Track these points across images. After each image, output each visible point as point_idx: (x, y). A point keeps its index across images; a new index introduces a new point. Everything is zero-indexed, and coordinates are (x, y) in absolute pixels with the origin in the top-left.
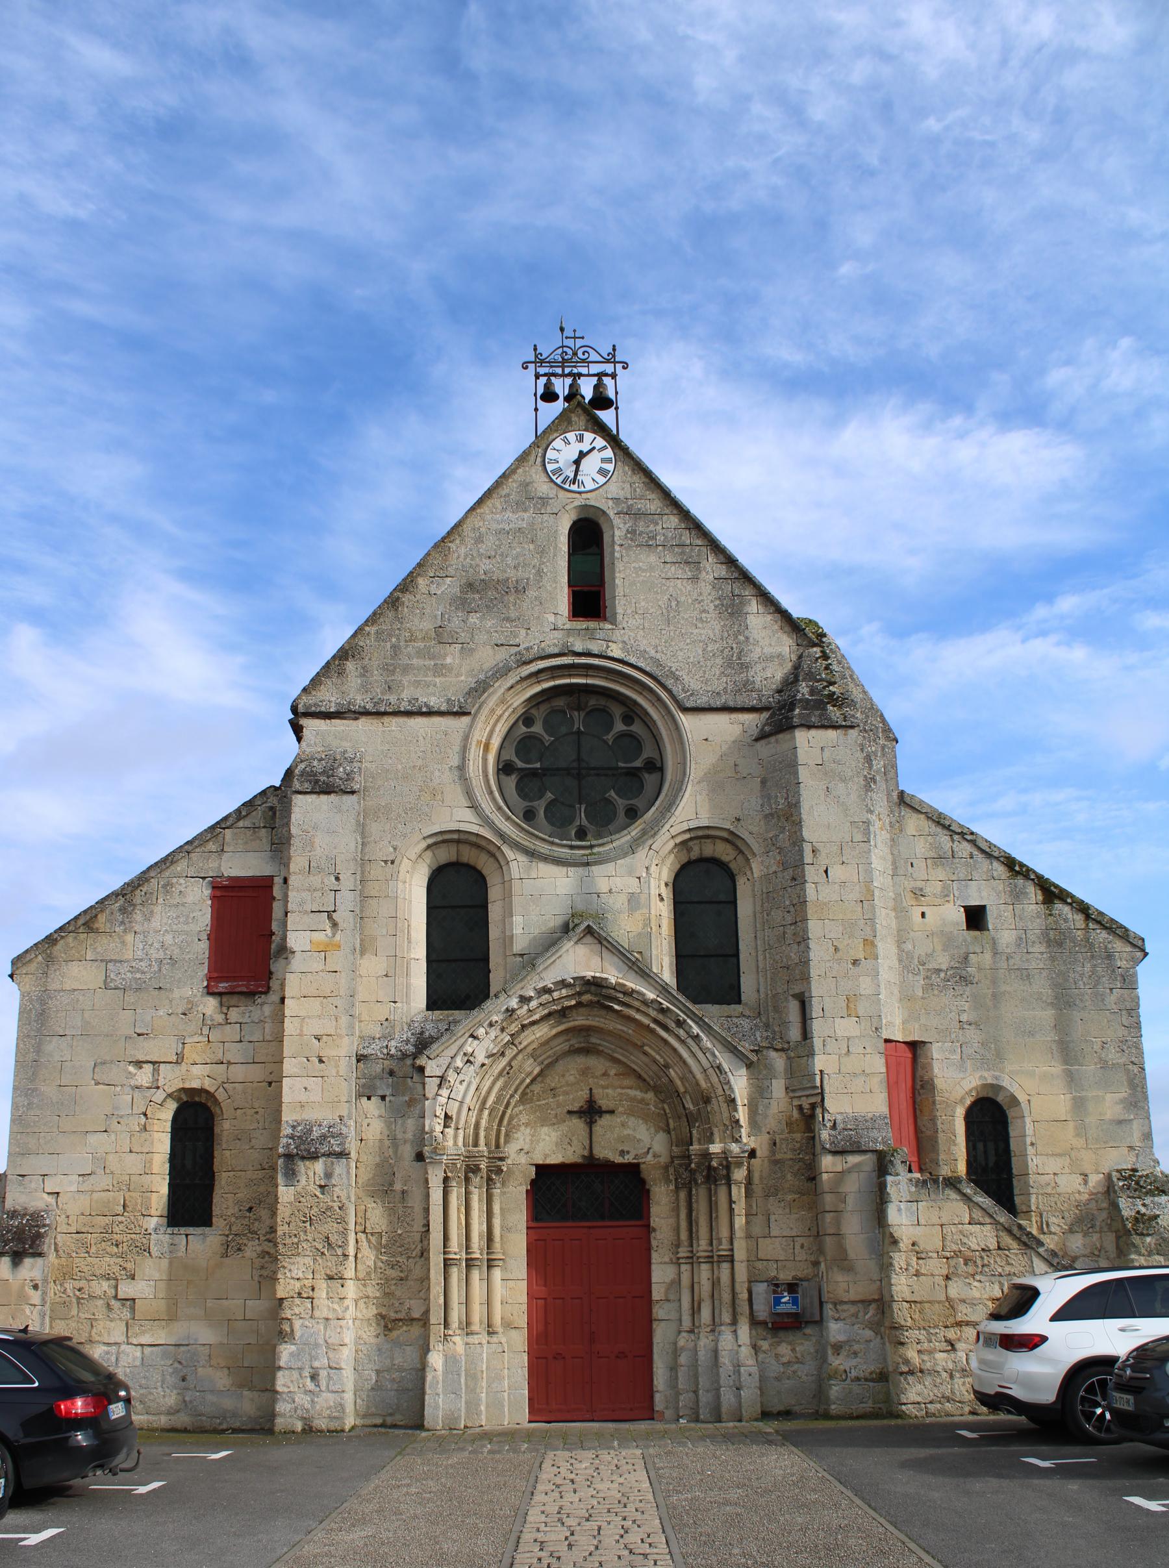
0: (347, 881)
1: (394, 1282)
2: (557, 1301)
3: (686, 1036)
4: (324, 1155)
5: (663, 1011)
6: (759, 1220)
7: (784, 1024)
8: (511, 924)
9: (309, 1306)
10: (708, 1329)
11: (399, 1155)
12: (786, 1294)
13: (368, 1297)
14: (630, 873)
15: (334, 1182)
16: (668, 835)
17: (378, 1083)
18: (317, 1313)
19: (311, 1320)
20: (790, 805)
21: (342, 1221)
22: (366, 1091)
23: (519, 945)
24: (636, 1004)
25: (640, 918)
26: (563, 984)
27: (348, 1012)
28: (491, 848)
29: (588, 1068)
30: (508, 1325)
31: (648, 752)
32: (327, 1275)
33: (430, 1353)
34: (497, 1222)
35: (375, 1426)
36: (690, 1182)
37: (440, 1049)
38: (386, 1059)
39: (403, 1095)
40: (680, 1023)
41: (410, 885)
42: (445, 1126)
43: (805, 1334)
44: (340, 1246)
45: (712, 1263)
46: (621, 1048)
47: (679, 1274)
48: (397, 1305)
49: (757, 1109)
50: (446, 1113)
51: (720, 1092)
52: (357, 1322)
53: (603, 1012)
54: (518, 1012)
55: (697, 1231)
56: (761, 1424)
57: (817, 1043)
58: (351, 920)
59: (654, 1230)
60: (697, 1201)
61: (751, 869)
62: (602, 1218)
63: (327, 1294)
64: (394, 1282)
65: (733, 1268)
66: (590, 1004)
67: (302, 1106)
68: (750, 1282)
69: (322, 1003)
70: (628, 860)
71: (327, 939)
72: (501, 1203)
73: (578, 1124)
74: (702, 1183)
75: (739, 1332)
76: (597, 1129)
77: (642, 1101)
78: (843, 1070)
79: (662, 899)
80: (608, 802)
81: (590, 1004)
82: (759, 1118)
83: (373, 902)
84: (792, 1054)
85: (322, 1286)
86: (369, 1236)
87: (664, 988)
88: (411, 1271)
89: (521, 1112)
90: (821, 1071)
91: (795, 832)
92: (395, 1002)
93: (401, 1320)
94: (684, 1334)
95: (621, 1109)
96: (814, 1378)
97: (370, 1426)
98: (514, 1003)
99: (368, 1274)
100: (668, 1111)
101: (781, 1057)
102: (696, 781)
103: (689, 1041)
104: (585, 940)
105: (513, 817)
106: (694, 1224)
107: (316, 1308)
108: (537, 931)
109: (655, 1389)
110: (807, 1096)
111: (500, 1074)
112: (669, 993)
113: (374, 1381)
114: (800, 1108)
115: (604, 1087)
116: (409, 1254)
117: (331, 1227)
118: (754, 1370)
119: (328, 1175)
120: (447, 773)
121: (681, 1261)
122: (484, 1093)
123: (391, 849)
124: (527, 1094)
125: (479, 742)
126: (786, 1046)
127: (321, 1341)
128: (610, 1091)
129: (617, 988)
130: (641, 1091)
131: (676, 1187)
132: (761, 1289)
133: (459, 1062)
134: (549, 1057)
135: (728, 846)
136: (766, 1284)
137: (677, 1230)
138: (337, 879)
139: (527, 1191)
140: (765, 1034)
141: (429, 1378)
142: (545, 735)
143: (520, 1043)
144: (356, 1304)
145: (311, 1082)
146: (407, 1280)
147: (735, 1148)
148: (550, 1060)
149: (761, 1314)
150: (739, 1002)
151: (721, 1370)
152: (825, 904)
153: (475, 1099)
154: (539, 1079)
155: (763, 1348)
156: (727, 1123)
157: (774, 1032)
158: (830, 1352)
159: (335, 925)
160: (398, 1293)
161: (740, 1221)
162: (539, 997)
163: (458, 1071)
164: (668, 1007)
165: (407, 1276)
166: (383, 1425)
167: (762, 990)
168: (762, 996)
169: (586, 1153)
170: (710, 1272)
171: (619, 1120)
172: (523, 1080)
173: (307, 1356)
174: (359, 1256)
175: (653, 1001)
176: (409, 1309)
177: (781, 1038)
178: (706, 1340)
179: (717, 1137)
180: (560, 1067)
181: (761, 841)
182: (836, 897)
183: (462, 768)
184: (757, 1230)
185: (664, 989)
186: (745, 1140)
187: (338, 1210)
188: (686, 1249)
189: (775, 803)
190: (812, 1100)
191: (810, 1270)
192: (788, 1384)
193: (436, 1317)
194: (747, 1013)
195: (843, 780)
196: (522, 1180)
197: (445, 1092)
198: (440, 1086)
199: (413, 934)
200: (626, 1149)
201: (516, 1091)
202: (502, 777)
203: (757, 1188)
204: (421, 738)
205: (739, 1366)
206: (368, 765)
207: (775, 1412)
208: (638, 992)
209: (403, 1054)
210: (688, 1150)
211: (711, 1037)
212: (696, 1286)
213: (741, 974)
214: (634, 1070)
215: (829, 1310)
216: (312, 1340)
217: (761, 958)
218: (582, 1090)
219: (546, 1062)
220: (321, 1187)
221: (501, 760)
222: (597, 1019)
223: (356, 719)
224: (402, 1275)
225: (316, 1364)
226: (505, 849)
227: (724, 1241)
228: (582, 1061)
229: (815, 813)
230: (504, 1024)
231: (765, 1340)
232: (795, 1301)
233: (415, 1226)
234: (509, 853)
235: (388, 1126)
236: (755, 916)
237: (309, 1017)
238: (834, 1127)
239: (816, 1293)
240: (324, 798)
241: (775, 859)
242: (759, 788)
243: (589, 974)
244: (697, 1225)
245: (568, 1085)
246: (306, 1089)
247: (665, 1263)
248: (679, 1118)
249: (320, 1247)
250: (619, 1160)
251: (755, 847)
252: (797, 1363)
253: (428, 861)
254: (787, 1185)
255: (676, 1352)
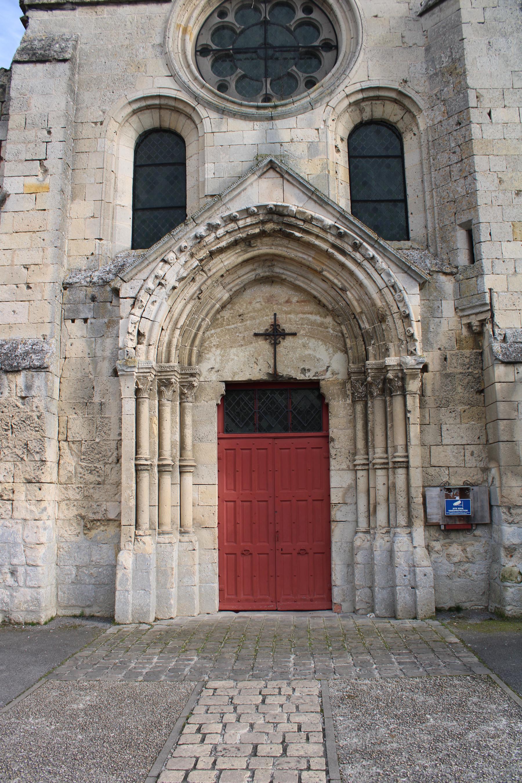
0: (58, 134)
1: (92, 486)
2: (245, 503)
3: (362, 259)
4: (24, 369)
5: (341, 236)
6: (432, 429)
7: (453, 251)
8: (204, 171)
9: (10, 507)
10: (384, 531)
11: (98, 370)
12: (458, 498)
13: (69, 499)
14: (310, 125)
15: (33, 393)
16: (343, 95)
17: (81, 307)
18: (16, 514)
19: (11, 521)
20: (454, 61)
21: (39, 429)
22: (71, 315)
23: (209, 189)
24: (316, 230)
25: (319, 162)
26: (247, 212)
27: (53, 244)
28: (188, 110)
29: (272, 296)
30: (200, 525)
31: (325, 34)
32: (26, 479)
33: (121, 552)
34: (189, 432)
35: (75, 616)
36: (366, 396)
37: (134, 272)
38: (89, 286)
39: (103, 317)
40: (356, 247)
41: (118, 144)
42: (139, 343)
43: (475, 536)
44: (38, 453)
45: (387, 469)
46: (302, 276)
47: (356, 480)
48: (95, 506)
49: (429, 328)
50: (139, 332)
51: (395, 309)
52: (60, 522)
53: (285, 242)
54: (206, 239)
55: (373, 440)
56: (436, 623)
57: (486, 264)
58: (60, 166)
59: (333, 440)
60: (373, 413)
61: (417, 125)
62: (286, 430)
63: (26, 496)
64: (92, 486)
65: (408, 474)
66: (273, 234)
67: (11, 327)
68: (424, 487)
69: (31, 237)
70: (307, 115)
71: (38, 183)
72: (193, 416)
73: (264, 345)
74: (378, 395)
75: (414, 534)
76: (281, 349)
77: (321, 325)
78: (511, 288)
79: (338, 151)
80: (290, 76)
81: (273, 234)
82: (430, 336)
83: (84, 156)
84: (461, 277)
85: (21, 489)
86: (71, 443)
87: (341, 214)
88: (107, 475)
89: (212, 335)
90: (490, 290)
91: (460, 82)
92: (100, 239)
93: (99, 520)
94: (360, 535)
95: (302, 332)
96: (483, 576)
97: (70, 616)
98: (202, 230)
99: (69, 478)
100: (345, 332)
101: (450, 280)
102: (367, 50)
103: (366, 264)
104: (268, 175)
105: (207, 85)
106: (370, 434)
107: (15, 509)
108: (226, 175)
109: (333, 584)
110: (476, 314)
111: (191, 298)
112: (346, 218)
113: (74, 576)
114: (469, 326)
115: (287, 313)
116: (106, 461)
117: (30, 435)
118: (429, 570)
119: (28, 387)
120: (150, 49)
121: (358, 467)
122: (176, 315)
123: (101, 113)
124: (218, 319)
125: (179, 26)
126: (455, 270)
127: (20, 540)
128: (292, 316)
129: (298, 216)
130: (321, 316)
131: (353, 401)
132: (434, 494)
133: (151, 284)
134: (237, 285)
135: (396, 107)
136: (439, 489)
137: (354, 440)
138: (49, 132)
139: (218, 405)
140: (434, 262)
141: (119, 575)
142: (236, 24)
143: (210, 270)
144: (59, 506)
145: (19, 307)
146: (104, 484)
147: (410, 360)
148: (238, 287)
149: (434, 516)
150: (408, 238)
151: (397, 569)
152: (490, 141)
153: (168, 320)
154: (229, 306)
155: (436, 549)
156: (402, 338)
157: (442, 260)
158: (503, 553)
159: (46, 171)
160: (96, 496)
161: (414, 430)
162: (226, 225)
163: (150, 292)
164: (345, 232)
165: (104, 480)
166: (82, 616)
167: (430, 225)
168: (430, 230)
169: (271, 371)
170: (386, 477)
171: (300, 342)
172: (214, 305)
173: (6, 554)
174: (62, 462)
175: (330, 227)
176: (106, 510)
177: (449, 264)
178: (381, 541)
179: (392, 351)
180: (248, 294)
181: (426, 98)
182: (499, 136)
183: (162, 45)
184: (430, 439)
185: (341, 215)
186: (419, 352)
187: (37, 419)
188: (362, 457)
189: (439, 63)
190: (482, 317)
191: (479, 476)
192: (459, 582)
193: (128, 518)
194: (416, 246)
195: (504, 35)
196: (213, 395)
197: (137, 311)
198: (133, 306)
199: (120, 185)
200: (307, 367)
201: (207, 315)
202: (200, 58)
203: (430, 401)
204: (128, 23)
205: (414, 566)
206: (84, 46)
207: (447, 608)
208: (317, 219)
209: (104, 282)
210: (364, 366)
211: (386, 259)
212: (372, 490)
213: (409, 215)
214: (315, 297)
215: (501, 514)
216: (11, 539)
217: (428, 197)
218: (267, 316)
219: (234, 289)
220: (23, 398)
221: (198, 45)
222: (280, 248)
223: (74, 9)
224: (99, 479)
225: (15, 561)
226: (199, 108)
227: (399, 448)
228: (266, 290)
229: (479, 65)
230: (194, 250)
231: (437, 540)
232: (466, 505)
233: (112, 435)
234: (202, 111)
235: (89, 346)
236: (421, 164)
237: (19, 249)
238: (505, 340)
239: (486, 497)
240: (40, 66)
241: (440, 110)
242: (424, 55)
243: (271, 203)
244: (373, 435)
245: (255, 311)
246: (14, 312)
247: (343, 470)
248: (356, 338)
249: (20, 453)
250: (300, 377)
251: (421, 103)
252: (467, 562)
253: (135, 126)
254: (457, 397)
255: (352, 551)
